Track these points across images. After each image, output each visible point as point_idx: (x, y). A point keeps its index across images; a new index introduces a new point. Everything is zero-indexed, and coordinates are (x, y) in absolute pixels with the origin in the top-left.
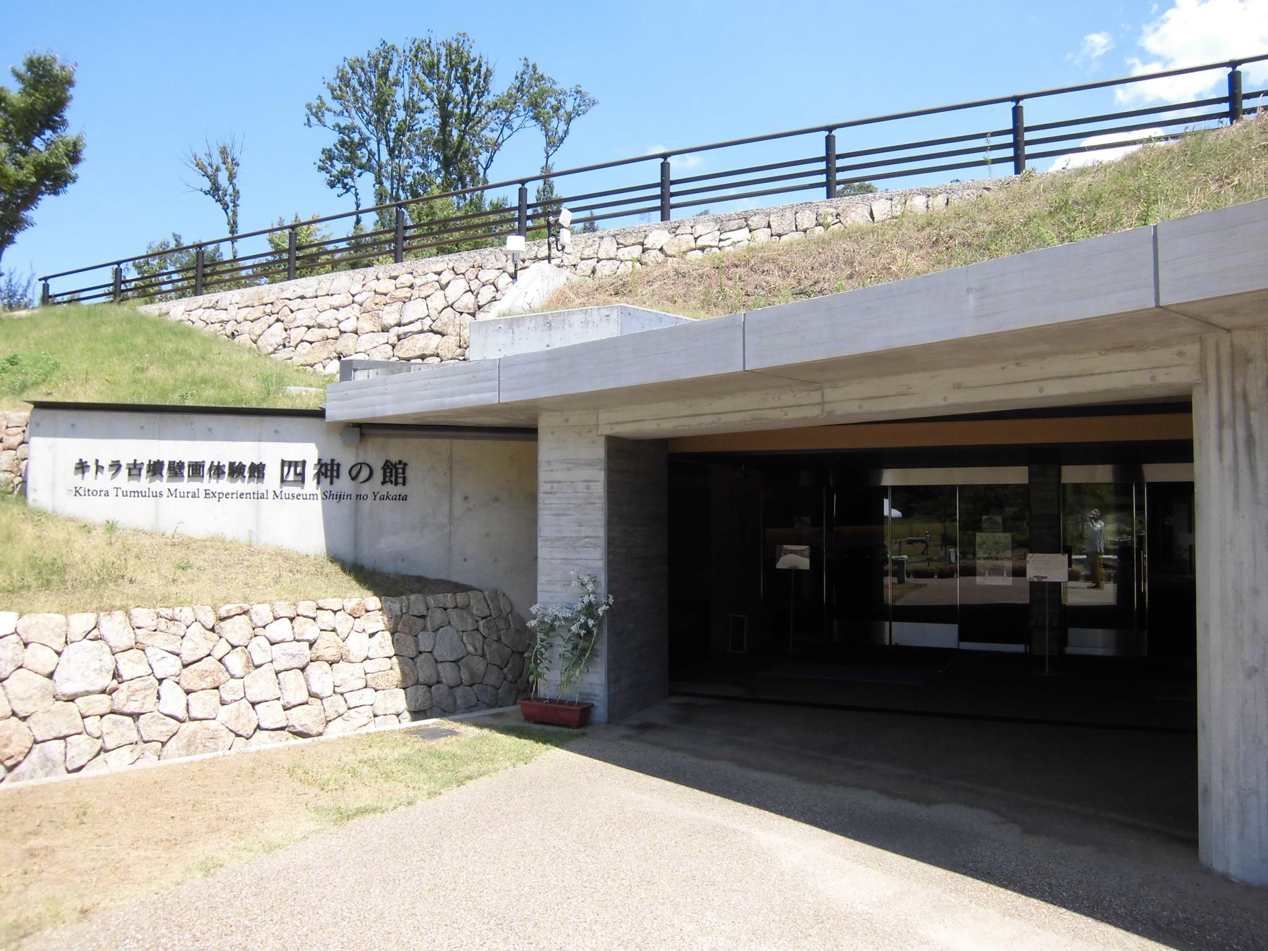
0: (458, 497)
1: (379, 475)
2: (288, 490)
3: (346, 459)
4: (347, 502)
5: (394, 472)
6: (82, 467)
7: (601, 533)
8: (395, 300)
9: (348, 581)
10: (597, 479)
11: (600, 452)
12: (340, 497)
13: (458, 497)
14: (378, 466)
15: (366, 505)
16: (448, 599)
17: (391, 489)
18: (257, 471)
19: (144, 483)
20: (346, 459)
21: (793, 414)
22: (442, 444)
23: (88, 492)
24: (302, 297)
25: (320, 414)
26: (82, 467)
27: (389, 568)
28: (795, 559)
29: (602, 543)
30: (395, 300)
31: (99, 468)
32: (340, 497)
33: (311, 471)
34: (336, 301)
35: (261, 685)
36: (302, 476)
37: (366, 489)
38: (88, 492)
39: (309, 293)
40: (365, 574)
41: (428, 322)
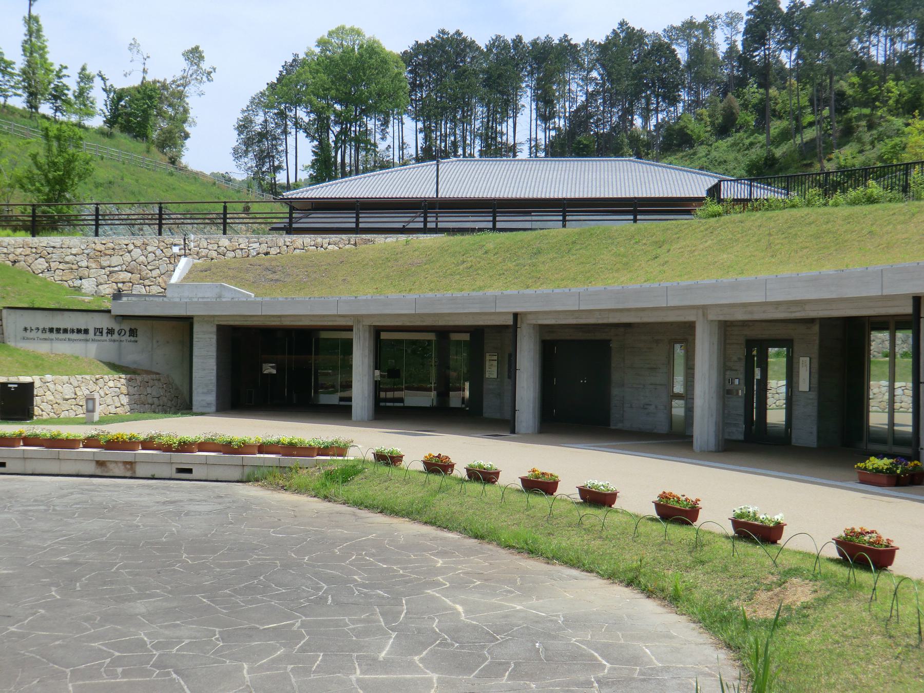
0: (154, 341)
1: (128, 333)
2: (97, 338)
3: (117, 328)
4: (117, 343)
5: (133, 332)
6: (26, 329)
7: (215, 354)
8: (106, 255)
9: (106, 369)
10: (214, 338)
11: (215, 329)
12: (114, 341)
13: (154, 341)
14: (127, 330)
15: (123, 344)
16: (154, 376)
17: (132, 339)
18: (86, 331)
19: (48, 335)
20: (117, 328)
21: (273, 323)
22: (149, 322)
23: (28, 339)
24: (54, 247)
25: (109, 311)
26: (26, 329)
27: (133, 366)
28: (269, 369)
29: (215, 357)
30: (106, 255)
31: (32, 330)
32: (114, 341)
33: (105, 331)
34: (74, 251)
35: (109, 401)
36: (101, 333)
37: (123, 338)
38: (28, 339)
39: (58, 245)
40: (116, 367)
41: (124, 267)
